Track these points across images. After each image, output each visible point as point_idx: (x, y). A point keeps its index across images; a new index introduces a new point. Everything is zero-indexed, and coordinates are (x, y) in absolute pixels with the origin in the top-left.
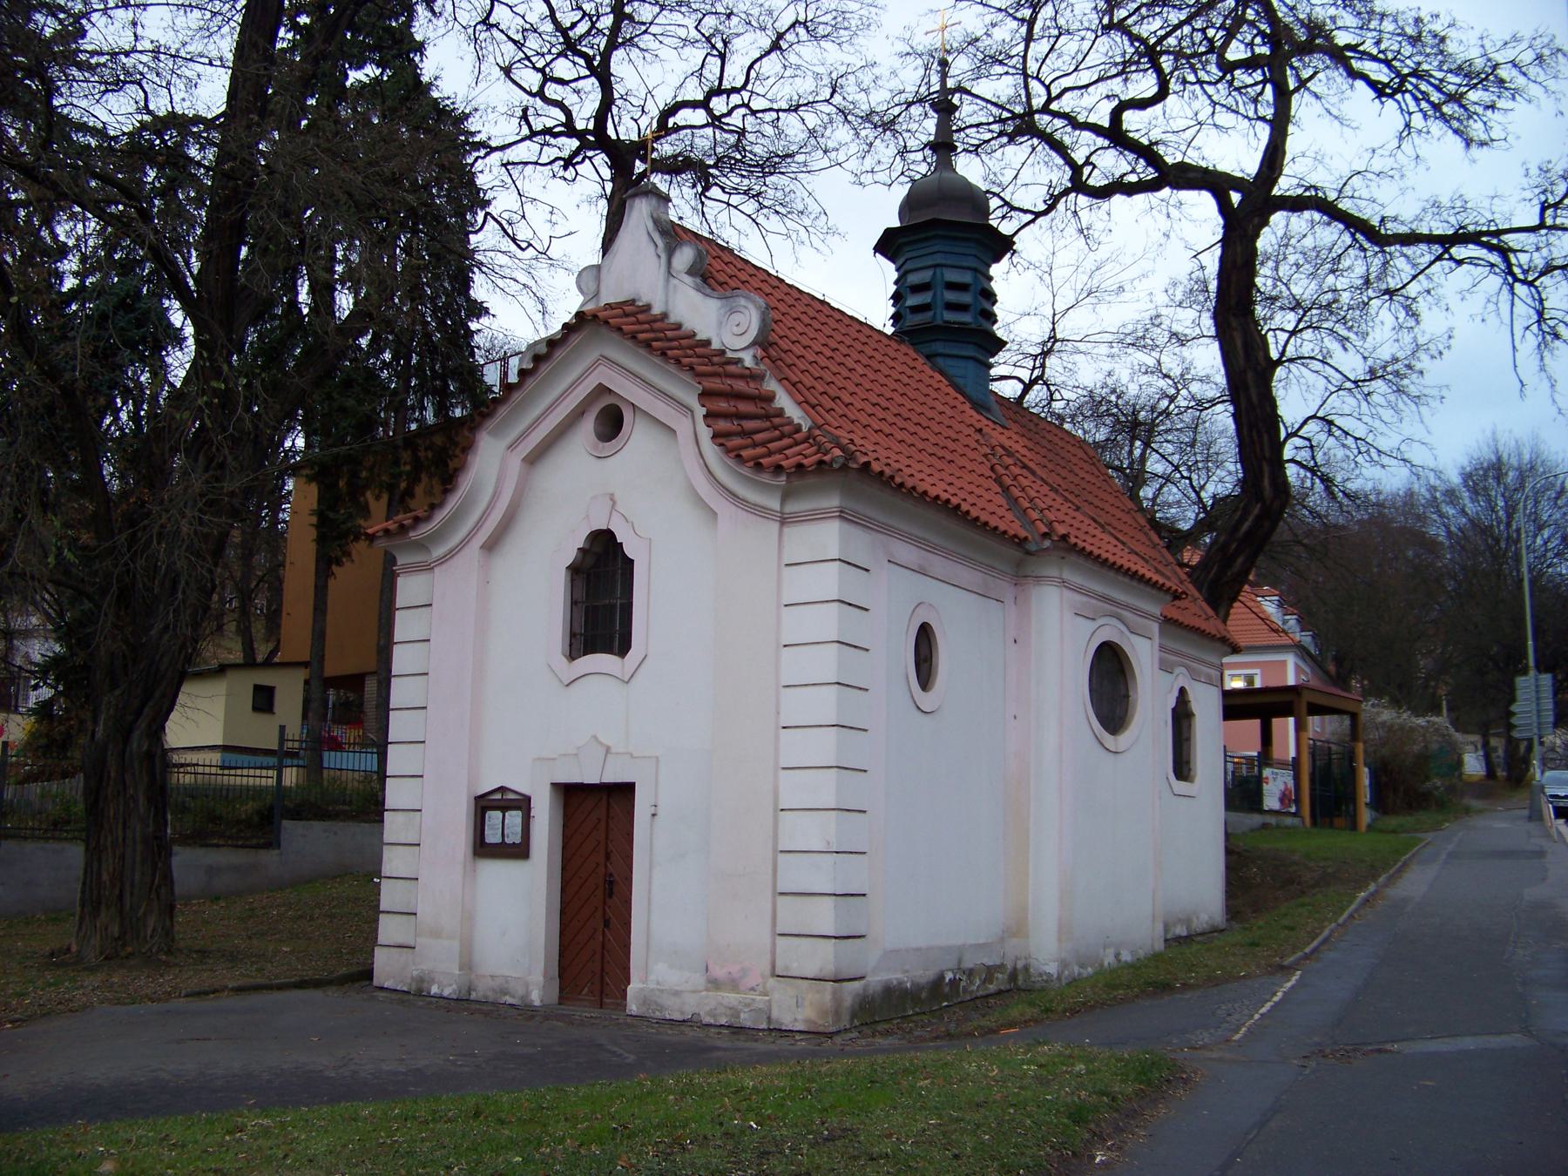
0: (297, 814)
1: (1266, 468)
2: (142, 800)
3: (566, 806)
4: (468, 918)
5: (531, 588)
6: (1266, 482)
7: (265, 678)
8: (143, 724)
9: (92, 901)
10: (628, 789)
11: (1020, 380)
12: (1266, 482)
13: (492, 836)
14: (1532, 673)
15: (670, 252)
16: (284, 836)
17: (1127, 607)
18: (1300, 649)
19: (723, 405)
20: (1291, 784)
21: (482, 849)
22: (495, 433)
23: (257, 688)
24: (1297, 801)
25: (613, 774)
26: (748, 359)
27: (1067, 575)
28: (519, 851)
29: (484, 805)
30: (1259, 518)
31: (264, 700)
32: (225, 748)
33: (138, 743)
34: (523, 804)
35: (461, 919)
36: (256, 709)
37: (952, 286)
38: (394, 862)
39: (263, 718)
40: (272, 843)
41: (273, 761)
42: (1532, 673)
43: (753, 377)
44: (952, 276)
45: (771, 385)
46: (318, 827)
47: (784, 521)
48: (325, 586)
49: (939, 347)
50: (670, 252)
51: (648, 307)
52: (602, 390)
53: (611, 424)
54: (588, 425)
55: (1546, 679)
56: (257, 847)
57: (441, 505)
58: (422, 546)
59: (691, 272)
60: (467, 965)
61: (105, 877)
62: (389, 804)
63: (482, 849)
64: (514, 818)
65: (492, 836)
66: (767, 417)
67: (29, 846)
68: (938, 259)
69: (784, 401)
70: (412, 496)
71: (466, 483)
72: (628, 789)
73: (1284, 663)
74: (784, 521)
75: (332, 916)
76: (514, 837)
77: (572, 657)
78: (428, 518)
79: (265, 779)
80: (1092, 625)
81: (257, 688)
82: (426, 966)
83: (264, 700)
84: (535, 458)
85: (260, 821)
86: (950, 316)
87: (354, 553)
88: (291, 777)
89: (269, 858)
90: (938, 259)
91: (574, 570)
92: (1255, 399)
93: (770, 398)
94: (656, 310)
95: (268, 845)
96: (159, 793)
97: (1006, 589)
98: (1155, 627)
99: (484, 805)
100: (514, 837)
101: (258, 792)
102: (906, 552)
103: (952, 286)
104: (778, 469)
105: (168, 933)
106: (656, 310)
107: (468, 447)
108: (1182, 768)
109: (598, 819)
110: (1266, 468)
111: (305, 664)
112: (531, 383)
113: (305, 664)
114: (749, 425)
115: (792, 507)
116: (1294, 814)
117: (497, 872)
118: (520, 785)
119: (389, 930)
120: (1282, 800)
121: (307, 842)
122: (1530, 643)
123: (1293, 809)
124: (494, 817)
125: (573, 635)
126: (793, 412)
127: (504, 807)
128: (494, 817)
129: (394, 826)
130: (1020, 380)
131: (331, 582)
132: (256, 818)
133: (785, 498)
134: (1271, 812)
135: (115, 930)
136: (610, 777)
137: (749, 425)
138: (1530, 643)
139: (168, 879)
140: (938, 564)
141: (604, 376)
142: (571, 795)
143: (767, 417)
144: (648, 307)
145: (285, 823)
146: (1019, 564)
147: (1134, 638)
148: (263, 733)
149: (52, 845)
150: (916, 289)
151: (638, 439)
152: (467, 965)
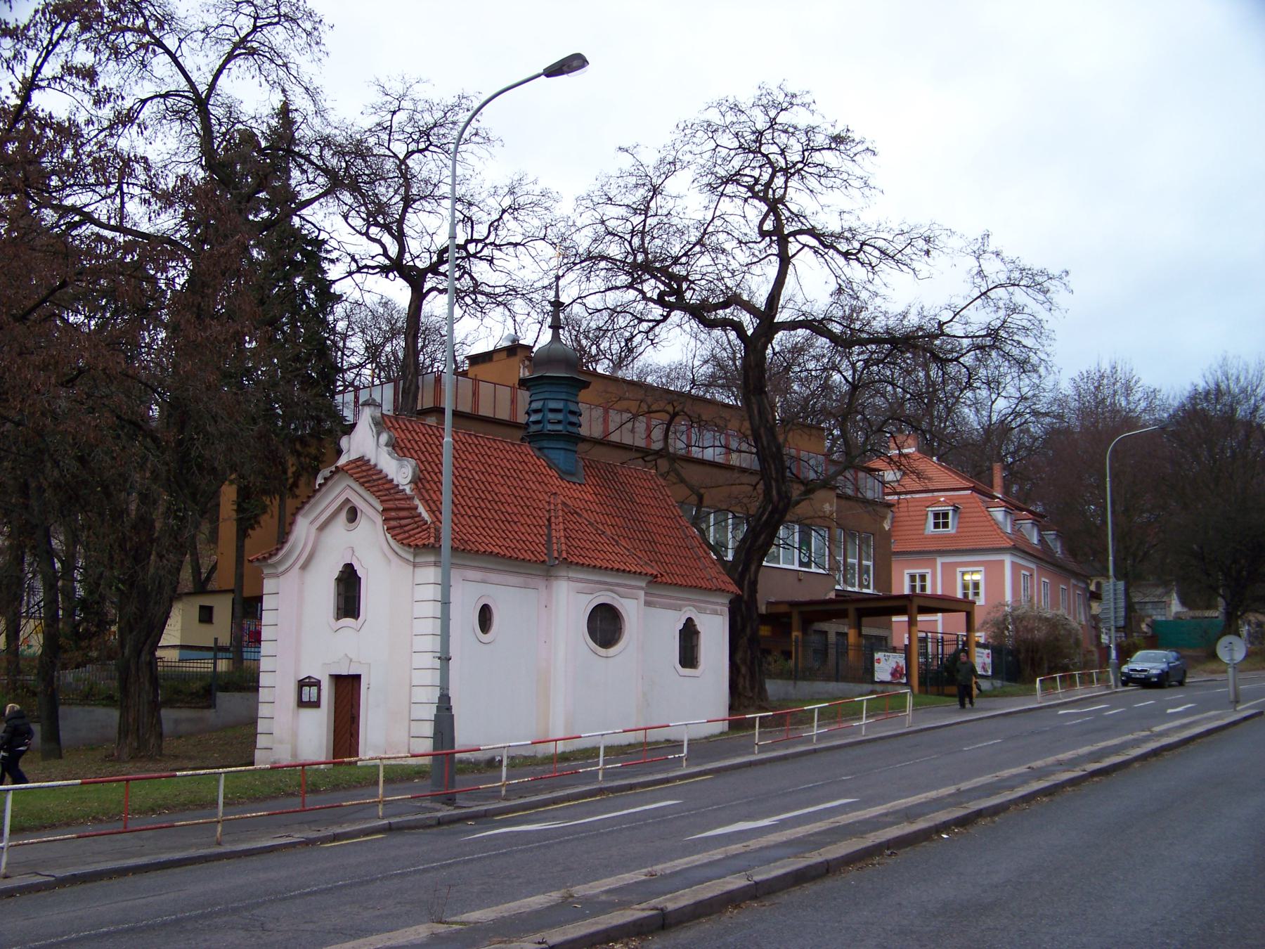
0: (226, 688)
1: (773, 484)
2: (147, 684)
3: (336, 685)
4: (295, 734)
5: (321, 588)
6: (774, 493)
7: (206, 601)
8: (146, 648)
9: (124, 731)
10: (358, 677)
11: (668, 412)
12: (774, 493)
13: (305, 699)
14: (1112, 580)
15: (379, 434)
16: (218, 702)
17: (618, 585)
18: (1019, 549)
19: (393, 514)
20: (902, 663)
21: (301, 704)
22: (305, 516)
23: (202, 607)
24: (908, 675)
25: (353, 671)
26: (408, 491)
27: (571, 575)
28: (316, 704)
29: (302, 684)
30: (772, 513)
31: (206, 615)
32: (182, 647)
33: (145, 657)
34: (318, 684)
35: (292, 733)
36: (201, 621)
37: (552, 410)
38: (263, 710)
39: (205, 627)
40: (211, 705)
41: (211, 654)
42: (1112, 580)
43: (411, 498)
44: (552, 405)
45: (417, 502)
46: (237, 695)
47: (415, 565)
48: (243, 546)
49: (545, 444)
50: (379, 434)
51: (369, 461)
52: (347, 500)
53: (353, 515)
54: (343, 515)
55: (1121, 585)
56: (203, 708)
57: (281, 548)
58: (274, 566)
59: (387, 445)
60: (294, 755)
61: (131, 720)
62: (261, 683)
63: (301, 704)
64: (314, 690)
65: (305, 699)
66: (413, 517)
67: (75, 709)
68: (547, 395)
69: (421, 509)
70: (297, 487)
71: (292, 538)
72: (358, 677)
73: (1002, 561)
74: (415, 565)
75: (242, 743)
76: (314, 699)
77: (338, 619)
78: (276, 554)
79: (205, 666)
80: (591, 597)
81: (202, 607)
82: (277, 757)
83: (206, 615)
84: (322, 528)
85: (204, 692)
86: (550, 427)
87: (262, 523)
88: (223, 666)
89: (209, 714)
90: (547, 395)
91: (339, 580)
92: (765, 443)
93: (416, 508)
94: (372, 463)
95: (209, 707)
96: (154, 679)
97: (540, 583)
98: (642, 593)
99: (302, 684)
100: (314, 699)
101: (201, 676)
102: (478, 575)
103: (552, 410)
104: (410, 546)
105: (160, 746)
106: (372, 463)
107: (292, 523)
108: (689, 657)
109: (347, 687)
110: (773, 484)
111: (232, 591)
112: (324, 489)
113: (232, 591)
114: (404, 522)
115: (418, 560)
116: (906, 684)
117: (307, 713)
118: (317, 675)
119: (261, 741)
120: (893, 674)
121: (228, 702)
122: (1111, 558)
123: (904, 681)
124: (306, 689)
125: (338, 609)
126: (425, 515)
127: (310, 685)
128: (306, 689)
129: (263, 694)
130: (668, 412)
131: (247, 541)
132: (202, 691)
133: (415, 556)
134: (882, 682)
135: (135, 744)
136: (352, 672)
137: (404, 522)
138: (1111, 558)
139: (159, 722)
140: (493, 577)
141: (349, 494)
142: (338, 679)
143: (413, 517)
144: (369, 461)
145: (219, 694)
146: (548, 571)
147: (623, 600)
148: (205, 636)
149: (87, 708)
150: (536, 411)
151: (363, 523)
152: (294, 755)
